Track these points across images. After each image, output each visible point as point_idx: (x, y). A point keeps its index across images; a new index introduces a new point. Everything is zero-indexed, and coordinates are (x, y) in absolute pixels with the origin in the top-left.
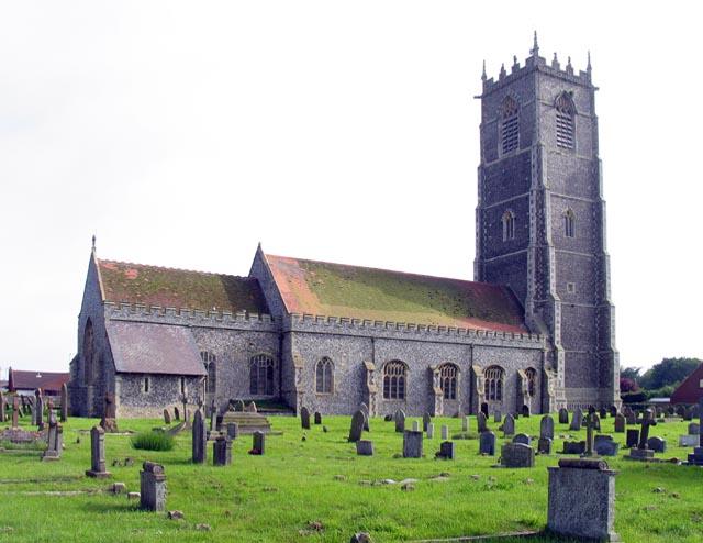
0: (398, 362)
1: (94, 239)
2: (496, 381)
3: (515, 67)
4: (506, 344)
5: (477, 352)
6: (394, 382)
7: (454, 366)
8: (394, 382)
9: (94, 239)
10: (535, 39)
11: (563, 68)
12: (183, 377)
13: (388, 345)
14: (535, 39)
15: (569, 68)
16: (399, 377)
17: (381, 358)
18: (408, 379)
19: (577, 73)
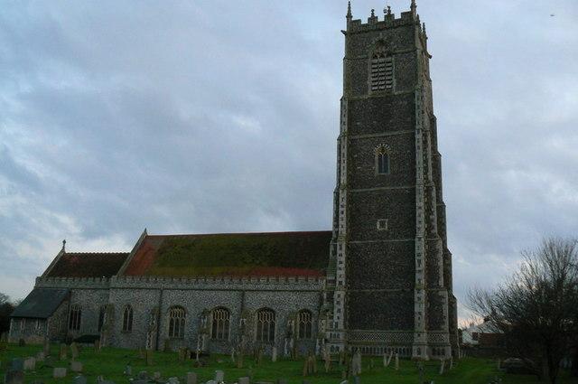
0: (180, 307)
1: (64, 242)
2: (224, 320)
3: (389, 16)
4: (279, 288)
5: (166, 294)
6: (177, 323)
7: (269, 310)
8: (177, 323)
9: (64, 242)
10: (349, 8)
11: (381, 18)
12: (39, 319)
13: (173, 294)
14: (349, 8)
15: (389, 16)
16: (441, 348)
17: (167, 304)
18: (187, 320)
19: (398, 16)
